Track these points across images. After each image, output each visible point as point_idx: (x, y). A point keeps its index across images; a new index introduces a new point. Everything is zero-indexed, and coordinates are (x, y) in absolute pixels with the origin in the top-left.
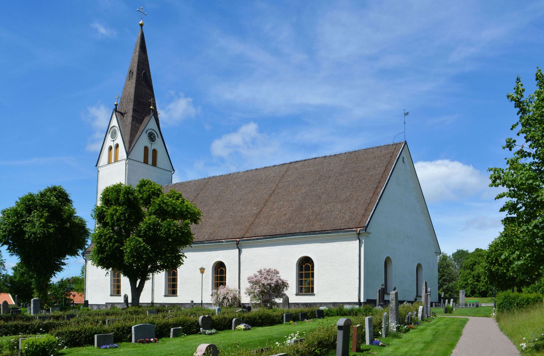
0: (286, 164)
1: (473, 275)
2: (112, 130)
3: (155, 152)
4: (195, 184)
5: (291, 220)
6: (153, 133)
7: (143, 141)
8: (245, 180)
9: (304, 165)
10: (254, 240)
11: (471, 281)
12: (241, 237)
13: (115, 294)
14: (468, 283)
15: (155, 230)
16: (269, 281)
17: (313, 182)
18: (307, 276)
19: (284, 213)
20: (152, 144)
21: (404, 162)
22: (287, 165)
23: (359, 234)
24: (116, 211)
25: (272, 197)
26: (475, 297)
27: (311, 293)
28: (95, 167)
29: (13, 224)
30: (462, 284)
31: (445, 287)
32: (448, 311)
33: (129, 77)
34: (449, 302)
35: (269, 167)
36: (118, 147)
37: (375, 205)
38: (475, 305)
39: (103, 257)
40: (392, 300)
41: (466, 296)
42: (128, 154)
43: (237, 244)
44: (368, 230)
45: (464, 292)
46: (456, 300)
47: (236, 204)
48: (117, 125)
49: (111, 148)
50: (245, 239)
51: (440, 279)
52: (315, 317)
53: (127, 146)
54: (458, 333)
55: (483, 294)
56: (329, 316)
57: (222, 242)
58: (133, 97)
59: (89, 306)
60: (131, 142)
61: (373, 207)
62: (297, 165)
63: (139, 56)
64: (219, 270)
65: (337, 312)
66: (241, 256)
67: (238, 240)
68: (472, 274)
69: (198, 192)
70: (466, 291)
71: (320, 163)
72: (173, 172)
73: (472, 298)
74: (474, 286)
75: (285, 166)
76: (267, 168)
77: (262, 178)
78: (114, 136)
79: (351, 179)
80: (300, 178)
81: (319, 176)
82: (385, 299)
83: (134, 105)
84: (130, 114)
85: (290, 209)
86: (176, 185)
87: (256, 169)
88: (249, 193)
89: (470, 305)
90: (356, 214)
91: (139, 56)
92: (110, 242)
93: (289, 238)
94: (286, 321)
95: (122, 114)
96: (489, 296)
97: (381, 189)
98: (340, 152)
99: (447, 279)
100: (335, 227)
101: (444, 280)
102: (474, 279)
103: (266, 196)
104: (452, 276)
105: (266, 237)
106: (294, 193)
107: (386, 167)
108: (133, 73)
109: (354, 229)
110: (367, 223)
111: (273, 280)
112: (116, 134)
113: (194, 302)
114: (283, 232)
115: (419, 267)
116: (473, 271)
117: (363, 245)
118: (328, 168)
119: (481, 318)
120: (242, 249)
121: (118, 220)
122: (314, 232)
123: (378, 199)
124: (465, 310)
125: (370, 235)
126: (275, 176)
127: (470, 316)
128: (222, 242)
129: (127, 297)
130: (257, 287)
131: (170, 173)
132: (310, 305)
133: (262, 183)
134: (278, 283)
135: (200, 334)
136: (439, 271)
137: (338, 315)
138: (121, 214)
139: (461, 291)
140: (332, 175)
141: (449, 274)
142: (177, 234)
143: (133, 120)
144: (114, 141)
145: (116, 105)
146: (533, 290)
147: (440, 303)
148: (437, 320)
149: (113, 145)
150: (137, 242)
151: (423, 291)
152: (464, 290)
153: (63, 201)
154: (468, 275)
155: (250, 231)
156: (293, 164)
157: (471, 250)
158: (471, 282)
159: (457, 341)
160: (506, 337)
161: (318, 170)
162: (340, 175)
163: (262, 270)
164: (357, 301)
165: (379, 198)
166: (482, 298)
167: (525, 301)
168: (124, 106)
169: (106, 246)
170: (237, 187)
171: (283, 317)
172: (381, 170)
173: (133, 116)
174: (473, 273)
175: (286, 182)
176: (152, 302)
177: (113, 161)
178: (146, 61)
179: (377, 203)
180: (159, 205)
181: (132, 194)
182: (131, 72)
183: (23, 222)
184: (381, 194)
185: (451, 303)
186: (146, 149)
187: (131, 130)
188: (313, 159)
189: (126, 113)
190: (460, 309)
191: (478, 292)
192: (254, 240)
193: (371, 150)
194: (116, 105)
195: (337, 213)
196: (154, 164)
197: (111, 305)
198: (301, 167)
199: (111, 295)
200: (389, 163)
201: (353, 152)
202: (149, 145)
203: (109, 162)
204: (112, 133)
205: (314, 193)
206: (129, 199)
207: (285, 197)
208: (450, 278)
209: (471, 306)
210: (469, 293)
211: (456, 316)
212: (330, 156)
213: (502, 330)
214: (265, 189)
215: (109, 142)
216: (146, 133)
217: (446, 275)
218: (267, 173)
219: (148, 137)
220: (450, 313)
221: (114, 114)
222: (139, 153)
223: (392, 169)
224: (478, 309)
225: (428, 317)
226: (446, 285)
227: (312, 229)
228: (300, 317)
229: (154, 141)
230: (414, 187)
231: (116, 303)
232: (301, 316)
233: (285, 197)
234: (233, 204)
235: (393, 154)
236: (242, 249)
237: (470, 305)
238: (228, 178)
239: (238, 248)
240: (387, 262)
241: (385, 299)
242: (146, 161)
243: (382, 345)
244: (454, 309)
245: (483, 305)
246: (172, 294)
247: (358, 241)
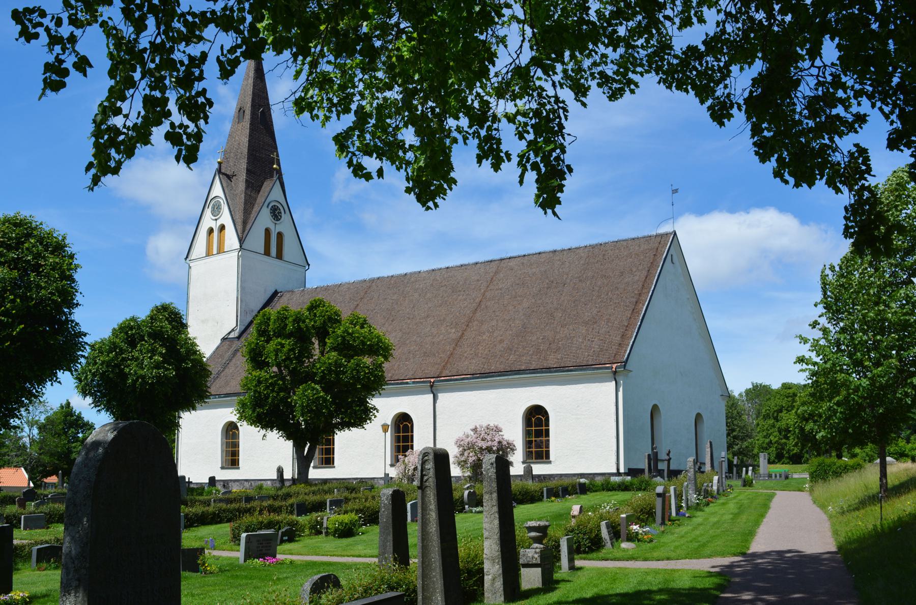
0: (495, 261)
1: (779, 428)
2: (213, 202)
3: (280, 235)
4: (349, 288)
5: (511, 350)
6: (278, 207)
7: (264, 219)
8: (432, 285)
9: (523, 263)
10: (456, 380)
11: (775, 437)
12: (436, 376)
13: (229, 465)
14: (771, 441)
15: (338, 374)
16: (489, 444)
17: (540, 291)
18: (539, 434)
19: (499, 338)
20: (276, 224)
21: (673, 263)
22: (496, 263)
23: (615, 373)
24: (283, 346)
25: (478, 314)
26: (783, 464)
27: (544, 460)
28: (184, 260)
29: (108, 364)
30: (763, 443)
31: (736, 448)
32: (747, 483)
33: (239, 117)
34: (747, 472)
35: (468, 265)
36: (224, 229)
37: (637, 329)
38: (783, 476)
39: (263, 413)
40: (690, 468)
41: (770, 462)
42: (241, 240)
43: (432, 386)
44: (628, 367)
45: (767, 456)
46: (756, 467)
47: (422, 323)
48: (222, 195)
49: (211, 231)
50: (443, 378)
51: (728, 435)
52: (577, 493)
53: (240, 228)
54: (766, 507)
55: (796, 459)
56: (591, 492)
57: (407, 383)
58: (245, 151)
59: (217, 484)
60: (245, 223)
61: (632, 333)
62: (512, 263)
63: (254, 85)
64: (401, 426)
65: (603, 485)
66: (437, 405)
67: (432, 380)
68: (777, 426)
69: (356, 303)
70: (769, 454)
71: (547, 261)
72: (307, 268)
73: (778, 465)
74: (781, 445)
75: (493, 263)
76: (466, 267)
77: (458, 283)
78: (217, 210)
79: (597, 289)
80: (518, 284)
81: (547, 281)
82: (659, 468)
83: (247, 163)
84: (242, 177)
85: (508, 333)
86: (318, 289)
87: (448, 268)
88: (441, 305)
89: (776, 476)
90: (609, 342)
91: (254, 86)
92: (273, 391)
93: (510, 377)
94: (547, 498)
95: (229, 177)
96: (805, 463)
97: (643, 305)
98: (577, 246)
99: (739, 436)
100: (579, 361)
101: (735, 437)
102: (780, 434)
103: (468, 312)
104: (747, 431)
105: (474, 376)
106: (511, 307)
107: (649, 271)
108: (244, 111)
109: (608, 365)
110: (626, 356)
111: (495, 440)
112: (221, 209)
113: (390, 476)
114: (501, 368)
115: (698, 417)
116: (777, 421)
117: (621, 389)
118: (561, 270)
119: (792, 492)
120: (439, 394)
121: (288, 358)
122: (549, 370)
123: (640, 321)
124: (769, 483)
125: (630, 374)
126: (478, 280)
127: (777, 490)
128: (407, 383)
129: (283, 470)
130: (471, 454)
131: (301, 269)
132: (544, 478)
133: (460, 291)
134: (502, 445)
135: (465, 512)
136: (727, 426)
137: (603, 490)
138: (290, 350)
139: (761, 455)
140: (568, 281)
141: (742, 428)
142: (369, 378)
143: (247, 188)
144: (216, 220)
145: (220, 163)
146: (873, 452)
147: (732, 473)
148: (736, 495)
149: (215, 226)
150: (313, 390)
151: (707, 456)
152: (766, 454)
153: (177, 327)
154: (771, 428)
155: (449, 366)
156: (505, 261)
157: (776, 385)
158: (776, 439)
159: (766, 513)
160: (819, 509)
161: (545, 271)
162: (580, 281)
163: (478, 426)
164: (615, 471)
165: (641, 318)
166: (794, 466)
167: (842, 468)
168: (231, 164)
169: (267, 397)
170: (420, 295)
171: (542, 493)
172: (640, 275)
173: (247, 181)
174: (778, 425)
175: (497, 290)
176: (292, 478)
177: (215, 252)
178: (264, 93)
179: (638, 326)
180: (343, 337)
181: (304, 322)
182: (241, 111)
183: (124, 359)
184: (643, 312)
185: (750, 473)
186: (268, 232)
187: (245, 203)
188: (536, 254)
189: (235, 175)
190: (762, 482)
191: (786, 455)
192: (456, 380)
193: (625, 243)
194: (220, 163)
195: (581, 340)
196: (279, 256)
197: (222, 483)
198: (519, 266)
199: (222, 468)
200: (653, 264)
201: (597, 245)
202: (272, 226)
203: (209, 253)
204: (213, 208)
205: (542, 308)
206: (300, 328)
207: (497, 313)
208: (744, 433)
209: (778, 477)
210: (772, 458)
211: (759, 489)
212: (563, 250)
213: (814, 502)
214: (465, 300)
215: (208, 221)
216: (268, 207)
217: (738, 429)
218: (466, 274)
219: (271, 213)
220: (750, 486)
221: (217, 177)
222: (256, 240)
223: (658, 274)
224: (787, 481)
225: (724, 491)
226: (737, 445)
227: (545, 365)
228: (560, 493)
229: (280, 219)
230: (688, 299)
231: (231, 481)
232: (562, 492)
233: (497, 313)
234: (416, 324)
235: (657, 251)
236: (439, 394)
237: (776, 476)
238: (403, 281)
239: (433, 393)
240: (655, 410)
241: (659, 468)
242: (267, 252)
243: (688, 517)
244: (754, 482)
245: (795, 476)
246: (232, 465)
247: (614, 382)
